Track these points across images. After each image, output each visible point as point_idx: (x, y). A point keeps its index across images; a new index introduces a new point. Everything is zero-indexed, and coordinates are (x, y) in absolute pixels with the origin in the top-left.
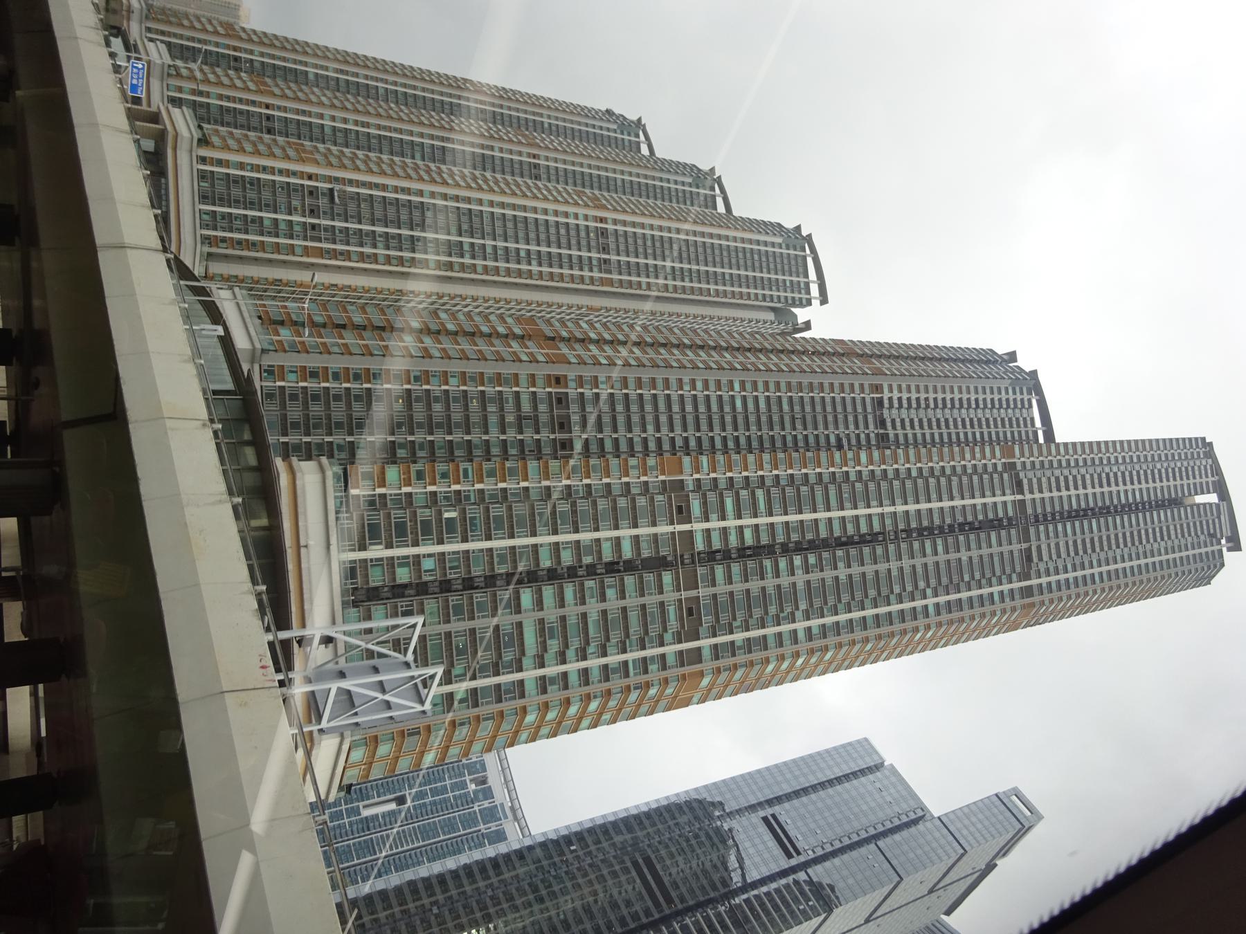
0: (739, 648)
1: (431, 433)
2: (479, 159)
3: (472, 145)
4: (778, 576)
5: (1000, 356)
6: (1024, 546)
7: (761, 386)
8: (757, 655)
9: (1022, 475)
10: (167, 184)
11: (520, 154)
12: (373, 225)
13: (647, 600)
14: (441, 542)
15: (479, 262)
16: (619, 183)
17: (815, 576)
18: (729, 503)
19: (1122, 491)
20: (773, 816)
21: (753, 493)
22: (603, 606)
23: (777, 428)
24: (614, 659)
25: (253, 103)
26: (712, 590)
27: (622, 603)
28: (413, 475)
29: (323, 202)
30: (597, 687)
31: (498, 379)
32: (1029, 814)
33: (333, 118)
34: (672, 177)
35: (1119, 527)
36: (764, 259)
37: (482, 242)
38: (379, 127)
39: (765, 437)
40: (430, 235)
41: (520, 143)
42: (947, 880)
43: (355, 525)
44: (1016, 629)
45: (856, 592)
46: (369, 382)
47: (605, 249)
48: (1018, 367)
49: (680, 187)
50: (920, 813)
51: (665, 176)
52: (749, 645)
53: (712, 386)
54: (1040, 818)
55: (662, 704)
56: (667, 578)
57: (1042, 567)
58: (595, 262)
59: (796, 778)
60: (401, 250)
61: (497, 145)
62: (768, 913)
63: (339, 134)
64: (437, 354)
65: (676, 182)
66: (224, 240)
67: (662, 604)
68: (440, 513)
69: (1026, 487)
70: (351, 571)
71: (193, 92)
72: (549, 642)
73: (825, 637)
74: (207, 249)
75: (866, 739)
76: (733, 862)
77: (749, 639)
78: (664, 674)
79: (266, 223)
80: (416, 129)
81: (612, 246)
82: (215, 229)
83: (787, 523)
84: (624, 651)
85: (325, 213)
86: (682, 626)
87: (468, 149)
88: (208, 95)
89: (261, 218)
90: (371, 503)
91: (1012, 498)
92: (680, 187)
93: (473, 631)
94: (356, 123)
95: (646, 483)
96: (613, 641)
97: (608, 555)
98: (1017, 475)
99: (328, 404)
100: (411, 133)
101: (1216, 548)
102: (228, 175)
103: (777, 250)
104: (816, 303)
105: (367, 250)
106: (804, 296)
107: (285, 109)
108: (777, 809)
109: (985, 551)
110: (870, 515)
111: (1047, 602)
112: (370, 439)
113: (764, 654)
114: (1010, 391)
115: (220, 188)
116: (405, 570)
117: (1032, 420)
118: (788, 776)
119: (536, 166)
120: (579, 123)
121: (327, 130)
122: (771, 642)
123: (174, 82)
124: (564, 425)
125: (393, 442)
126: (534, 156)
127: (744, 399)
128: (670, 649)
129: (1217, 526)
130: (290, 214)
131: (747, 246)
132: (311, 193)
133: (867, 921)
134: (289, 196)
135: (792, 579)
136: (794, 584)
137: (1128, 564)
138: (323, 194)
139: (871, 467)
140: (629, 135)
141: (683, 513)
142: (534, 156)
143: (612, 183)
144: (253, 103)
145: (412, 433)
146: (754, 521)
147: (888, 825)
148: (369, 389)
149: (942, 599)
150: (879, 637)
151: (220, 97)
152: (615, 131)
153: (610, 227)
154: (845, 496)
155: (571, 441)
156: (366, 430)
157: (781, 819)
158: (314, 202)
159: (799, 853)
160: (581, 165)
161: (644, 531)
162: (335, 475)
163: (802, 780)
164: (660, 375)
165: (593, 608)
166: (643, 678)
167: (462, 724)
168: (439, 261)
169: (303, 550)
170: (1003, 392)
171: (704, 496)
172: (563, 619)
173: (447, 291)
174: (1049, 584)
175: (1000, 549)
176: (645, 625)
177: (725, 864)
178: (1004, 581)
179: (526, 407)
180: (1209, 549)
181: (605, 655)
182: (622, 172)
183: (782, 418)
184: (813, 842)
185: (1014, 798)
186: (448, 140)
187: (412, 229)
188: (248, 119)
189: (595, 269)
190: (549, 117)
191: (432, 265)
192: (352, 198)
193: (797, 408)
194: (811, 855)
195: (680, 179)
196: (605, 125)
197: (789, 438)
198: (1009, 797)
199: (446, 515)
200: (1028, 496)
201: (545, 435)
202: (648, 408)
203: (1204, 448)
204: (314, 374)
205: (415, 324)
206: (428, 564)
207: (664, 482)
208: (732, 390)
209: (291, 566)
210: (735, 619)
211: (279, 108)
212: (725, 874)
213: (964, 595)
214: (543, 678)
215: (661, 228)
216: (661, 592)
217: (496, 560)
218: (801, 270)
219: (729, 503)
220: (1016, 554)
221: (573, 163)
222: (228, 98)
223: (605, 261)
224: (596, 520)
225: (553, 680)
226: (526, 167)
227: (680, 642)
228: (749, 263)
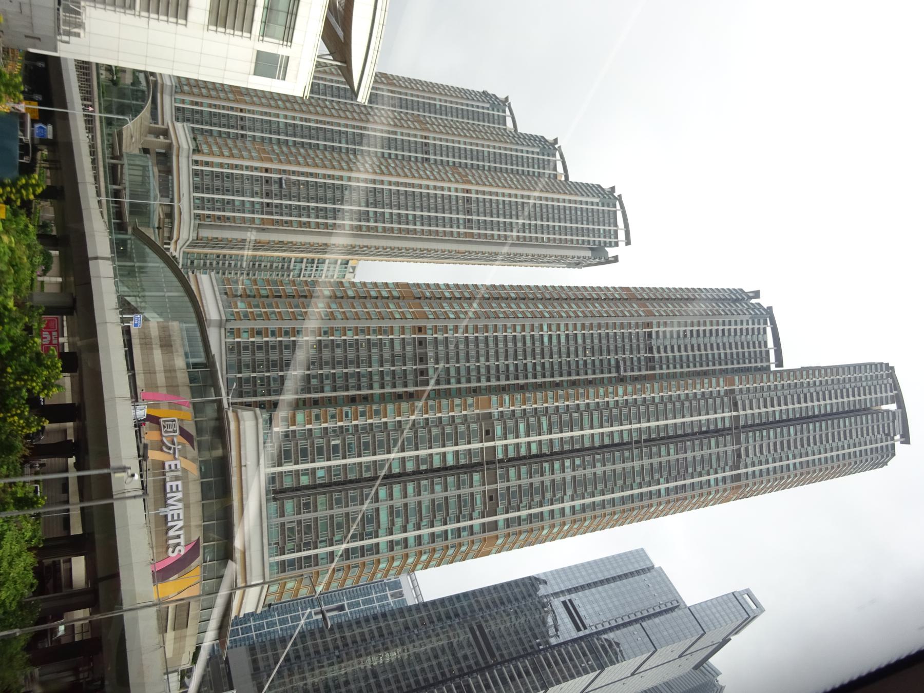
0: (524, 520)
1: (334, 368)
2: (386, 142)
3: (382, 131)
4: (553, 474)
5: (746, 293)
6: (736, 447)
7: (562, 327)
8: (535, 525)
9: (738, 397)
10: (172, 180)
11: (415, 136)
12: (308, 202)
13: (462, 491)
14: (329, 459)
15: (380, 225)
16: (486, 154)
17: (579, 473)
18: (522, 427)
19: (816, 405)
20: (570, 601)
21: (539, 419)
22: (432, 496)
23: (573, 356)
24: (438, 529)
25: (232, 109)
26: (506, 484)
27: (445, 494)
28: (313, 418)
29: (275, 188)
30: (426, 547)
31: (380, 331)
32: (754, 607)
33: (286, 117)
34: (525, 149)
35: (811, 432)
36: (585, 214)
37: (382, 210)
38: (317, 122)
39: (564, 362)
40: (346, 207)
41: (416, 128)
42: (692, 649)
43: (276, 452)
44: (728, 501)
45: (608, 482)
46: (294, 336)
47: (469, 212)
48: (759, 304)
49: (530, 155)
50: (675, 604)
51: (519, 148)
52: (530, 518)
53: (527, 329)
54: (762, 610)
55: (471, 554)
56: (476, 477)
57: (749, 461)
58: (461, 222)
59: (589, 575)
60: (326, 218)
61: (399, 130)
62: (564, 661)
63: (289, 128)
64: (339, 317)
65: (527, 152)
66: (209, 216)
67: (472, 494)
68: (329, 441)
69: (740, 406)
70: (272, 479)
71: (193, 103)
72: (396, 520)
73: (584, 512)
74: (197, 222)
75: (642, 549)
76: (550, 621)
77: (530, 515)
78: (472, 538)
79: (237, 203)
80: (343, 122)
81: (474, 209)
82: (203, 209)
83: (562, 438)
84: (445, 524)
85: (276, 195)
86: (485, 508)
87: (378, 134)
88: (201, 104)
89: (233, 200)
90: (286, 436)
91: (730, 414)
92: (530, 155)
93: (347, 514)
94: (301, 119)
95: (465, 416)
96: (438, 518)
97: (437, 463)
98: (735, 398)
99: (267, 352)
100: (339, 125)
101: (890, 443)
102: (212, 172)
103: (595, 207)
104: (622, 244)
105: (304, 219)
106: (613, 240)
107: (253, 112)
108: (573, 596)
109: (706, 452)
110: (622, 431)
111: (751, 485)
112: (294, 373)
113: (540, 524)
114: (750, 322)
115: (207, 181)
116: (306, 477)
117: (766, 343)
118: (584, 573)
119: (426, 144)
120: (462, 104)
121: (281, 125)
122: (546, 516)
123: (179, 97)
124: (423, 359)
125: (309, 375)
126: (426, 138)
127: (550, 336)
128: (477, 522)
129: (891, 428)
130: (253, 197)
131: (573, 205)
132: (267, 182)
133: (633, 674)
134: (252, 184)
135: (563, 475)
136: (564, 478)
137: (817, 457)
138: (275, 182)
139: (625, 398)
140: (498, 111)
141: (489, 435)
142: (426, 138)
143: (480, 154)
144: (232, 109)
145: (321, 369)
146: (539, 438)
147: (651, 611)
148: (294, 341)
149: (671, 485)
150: (624, 511)
151: (210, 106)
152: (488, 109)
153: (474, 196)
154: (605, 418)
155: (427, 369)
156: (291, 367)
157: (576, 603)
158: (268, 188)
159: (585, 628)
160: (459, 142)
161: (462, 447)
162: (265, 421)
163: (593, 576)
164: (490, 323)
165: (426, 497)
166: (457, 541)
167: (339, 570)
168: (352, 225)
169: (243, 468)
170: (745, 324)
171: (505, 423)
172: (406, 505)
173: (357, 244)
174: (754, 472)
175: (717, 450)
176: (460, 508)
177: (544, 623)
178: (719, 471)
179: (398, 348)
180: (884, 444)
181: (432, 526)
182: (489, 146)
183: (577, 348)
184: (596, 620)
185: (746, 596)
186: (365, 128)
187: (334, 204)
188: (228, 120)
189: (461, 226)
190: (440, 100)
191: (347, 228)
192: (294, 184)
193: (588, 341)
194: (594, 630)
195: (530, 149)
196: (481, 104)
197: (581, 362)
198: (742, 595)
199: (333, 443)
200: (742, 413)
201: (409, 367)
202: (482, 345)
203: (889, 370)
204: (259, 333)
205: (327, 293)
206: (320, 473)
207: (478, 414)
208: (542, 330)
209: (234, 479)
210: (521, 502)
211: (249, 111)
212: (544, 630)
213: (688, 482)
214: (391, 542)
215: (510, 195)
216: (472, 486)
217: (364, 469)
218: (612, 221)
219: (522, 427)
220: (729, 453)
221: (453, 141)
222: (215, 106)
223: (469, 220)
224: (430, 441)
225: (398, 543)
226: (419, 146)
227: (483, 517)
228: (573, 217)
